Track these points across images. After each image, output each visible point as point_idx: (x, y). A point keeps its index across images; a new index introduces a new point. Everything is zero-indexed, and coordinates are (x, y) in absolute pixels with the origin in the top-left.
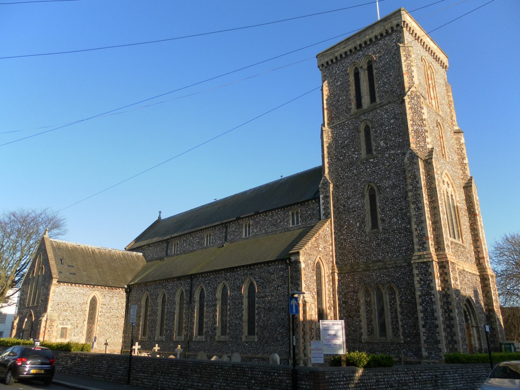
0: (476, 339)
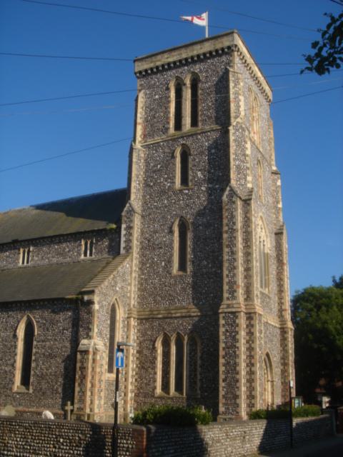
0: (270, 393)
